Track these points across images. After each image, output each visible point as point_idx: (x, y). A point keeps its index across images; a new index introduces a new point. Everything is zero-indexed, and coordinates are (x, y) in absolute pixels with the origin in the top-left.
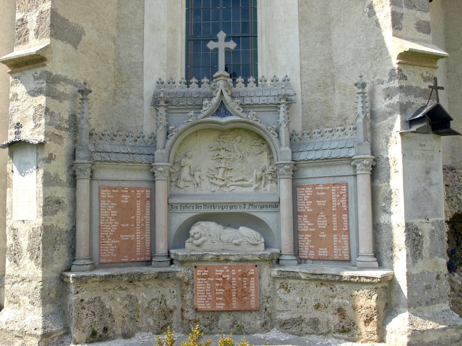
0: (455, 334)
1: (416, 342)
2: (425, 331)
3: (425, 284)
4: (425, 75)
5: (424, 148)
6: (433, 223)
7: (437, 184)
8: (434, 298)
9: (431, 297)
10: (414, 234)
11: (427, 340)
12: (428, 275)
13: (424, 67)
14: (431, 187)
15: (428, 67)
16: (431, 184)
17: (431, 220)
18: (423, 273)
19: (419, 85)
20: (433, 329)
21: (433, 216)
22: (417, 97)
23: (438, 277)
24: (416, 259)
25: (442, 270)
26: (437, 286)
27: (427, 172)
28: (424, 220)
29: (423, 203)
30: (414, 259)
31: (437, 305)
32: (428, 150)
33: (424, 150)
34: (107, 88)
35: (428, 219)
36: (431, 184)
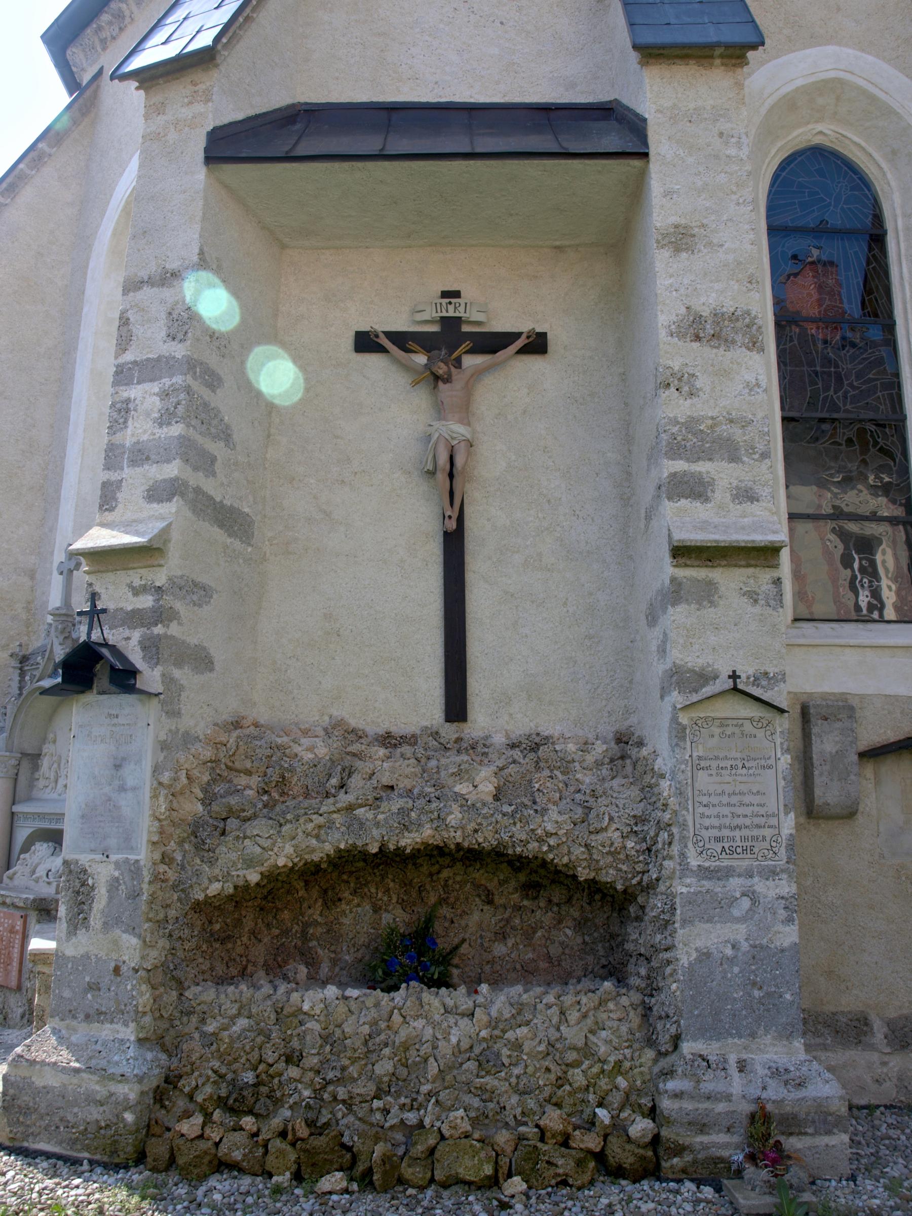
0: (98, 1088)
1: (18, 1079)
2: (38, 1062)
3: (87, 979)
4: (137, 583)
5: (115, 721)
6: (117, 865)
7: (134, 789)
8: (104, 1009)
9: (96, 1006)
10: (77, 881)
11: (39, 1082)
12: (96, 963)
13: (134, 568)
14: (123, 795)
15: (141, 568)
16: (122, 789)
17: (114, 857)
18: (87, 956)
19: (121, 605)
20: (55, 1063)
21: (119, 850)
22: (116, 627)
23: (117, 970)
24: (76, 928)
25: (126, 958)
26: (113, 989)
27: (117, 767)
28: (99, 857)
29: (102, 824)
30: (71, 928)
31: (108, 1025)
32: (123, 725)
33: (115, 725)
34: (8, 645)
35: (107, 857)
36: (122, 789)
